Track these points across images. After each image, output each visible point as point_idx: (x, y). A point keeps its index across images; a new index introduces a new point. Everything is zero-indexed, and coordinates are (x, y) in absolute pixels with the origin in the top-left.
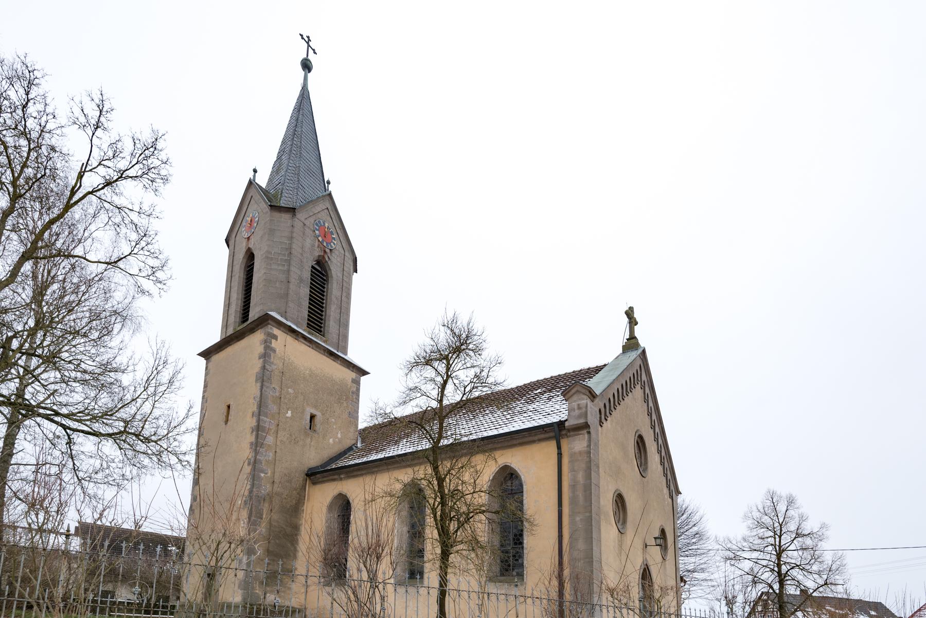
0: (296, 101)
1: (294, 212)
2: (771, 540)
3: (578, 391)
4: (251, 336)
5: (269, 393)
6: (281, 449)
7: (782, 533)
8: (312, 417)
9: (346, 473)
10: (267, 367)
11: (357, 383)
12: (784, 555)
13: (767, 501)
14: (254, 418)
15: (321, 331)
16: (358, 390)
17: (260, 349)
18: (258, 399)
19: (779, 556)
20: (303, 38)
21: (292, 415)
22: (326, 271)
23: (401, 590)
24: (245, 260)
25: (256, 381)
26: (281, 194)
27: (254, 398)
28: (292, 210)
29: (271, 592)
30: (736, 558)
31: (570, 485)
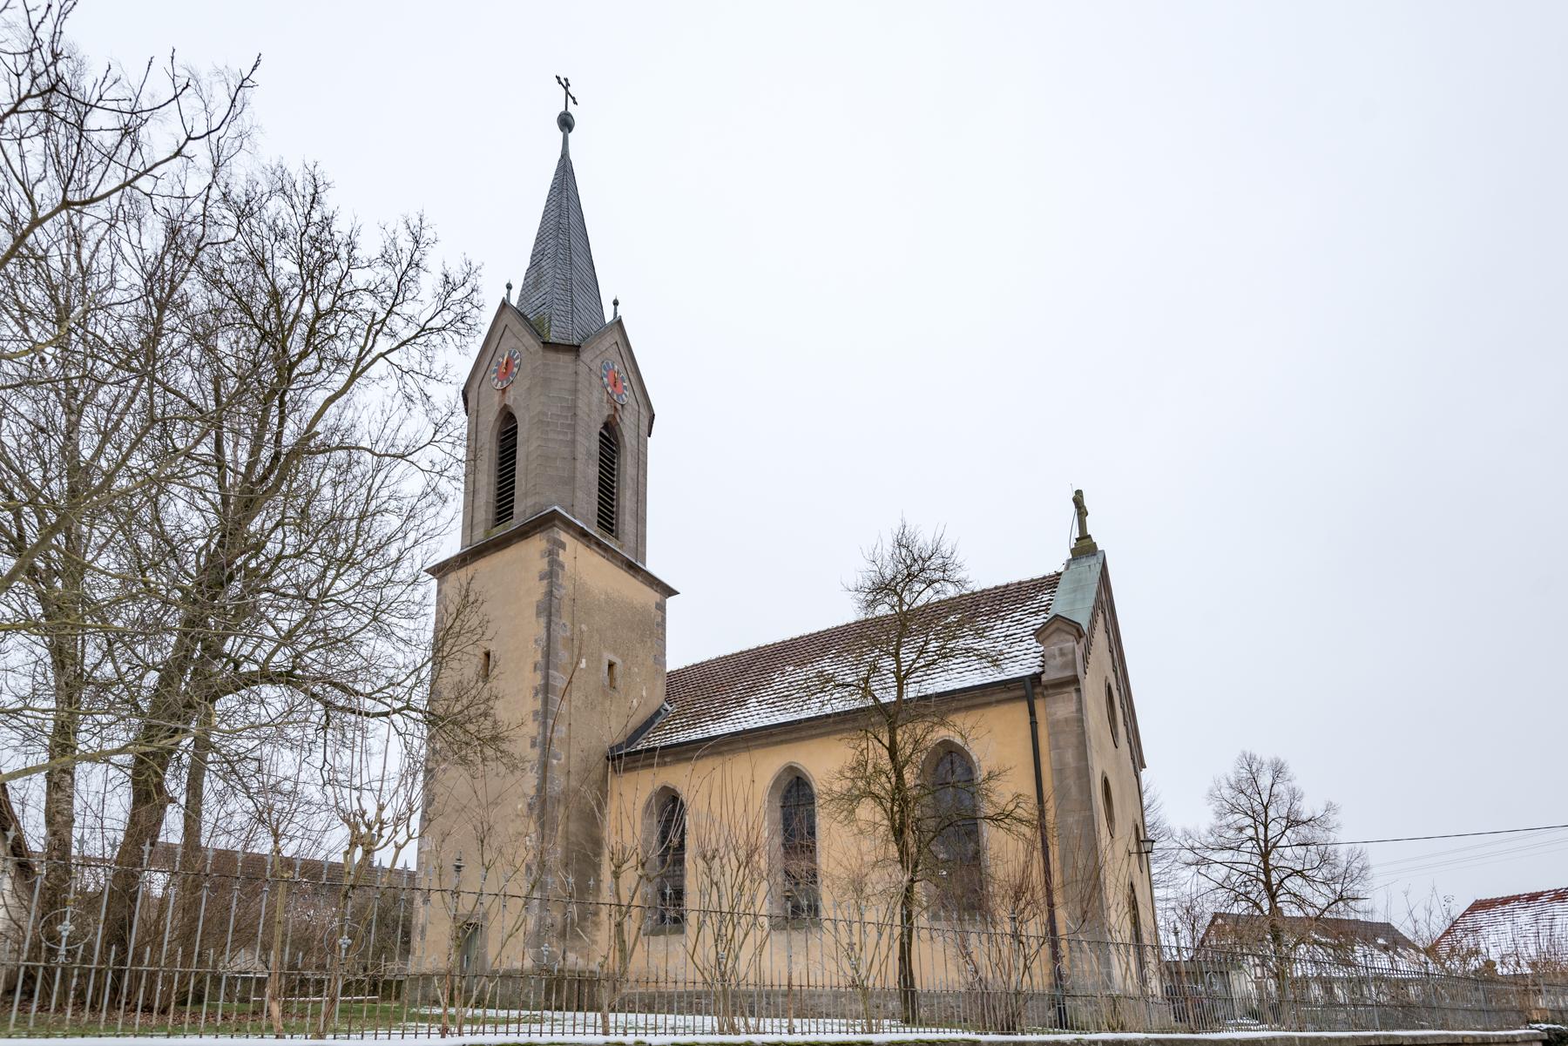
0: (552, 177)
1: (578, 351)
2: (1250, 832)
3: (1058, 629)
4: (523, 543)
5: (560, 634)
6: (575, 720)
7: (1269, 820)
8: (611, 665)
9: (676, 754)
10: (555, 592)
11: (661, 608)
12: (1274, 855)
13: (1242, 771)
14: (538, 672)
15: (612, 531)
16: (664, 619)
17: (543, 565)
18: (543, 643)
19: (1265, 855)
20: (560, 83)
21: (587, 666)
22: (616, 439)
23: (779, 938)
24: (498, 424)
25: (538, 614)
26: (550, 321)
27: (536, 641)
28: (575, 349)
29: (572, 949)
30: (1206, 862)
31: (1052, 770)
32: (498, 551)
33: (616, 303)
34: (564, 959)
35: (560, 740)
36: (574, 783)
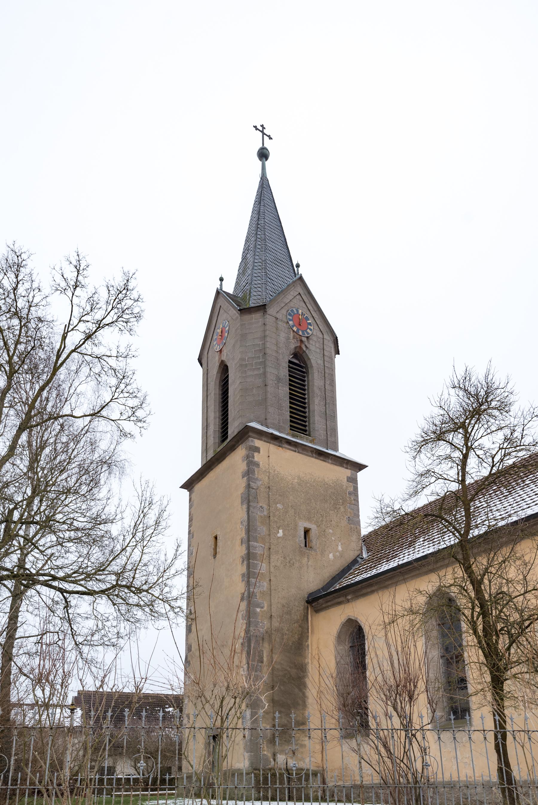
4: (232, 454)
5: (258, 514)
8: (307, 532)
9: (354, 592)
11: (354, 480)
14: (244, 545)
15: (306, 431)
16: (356, 489)
18: (245, 523)
21: (284, 534)
22: (305, 363)
25: (242, 503)
26: (250, 294)
27: (242, 523)
29: (282, 752)
32: (220, 463)
34: (274, 760)
35: (263, 593)
36: (276, 623)
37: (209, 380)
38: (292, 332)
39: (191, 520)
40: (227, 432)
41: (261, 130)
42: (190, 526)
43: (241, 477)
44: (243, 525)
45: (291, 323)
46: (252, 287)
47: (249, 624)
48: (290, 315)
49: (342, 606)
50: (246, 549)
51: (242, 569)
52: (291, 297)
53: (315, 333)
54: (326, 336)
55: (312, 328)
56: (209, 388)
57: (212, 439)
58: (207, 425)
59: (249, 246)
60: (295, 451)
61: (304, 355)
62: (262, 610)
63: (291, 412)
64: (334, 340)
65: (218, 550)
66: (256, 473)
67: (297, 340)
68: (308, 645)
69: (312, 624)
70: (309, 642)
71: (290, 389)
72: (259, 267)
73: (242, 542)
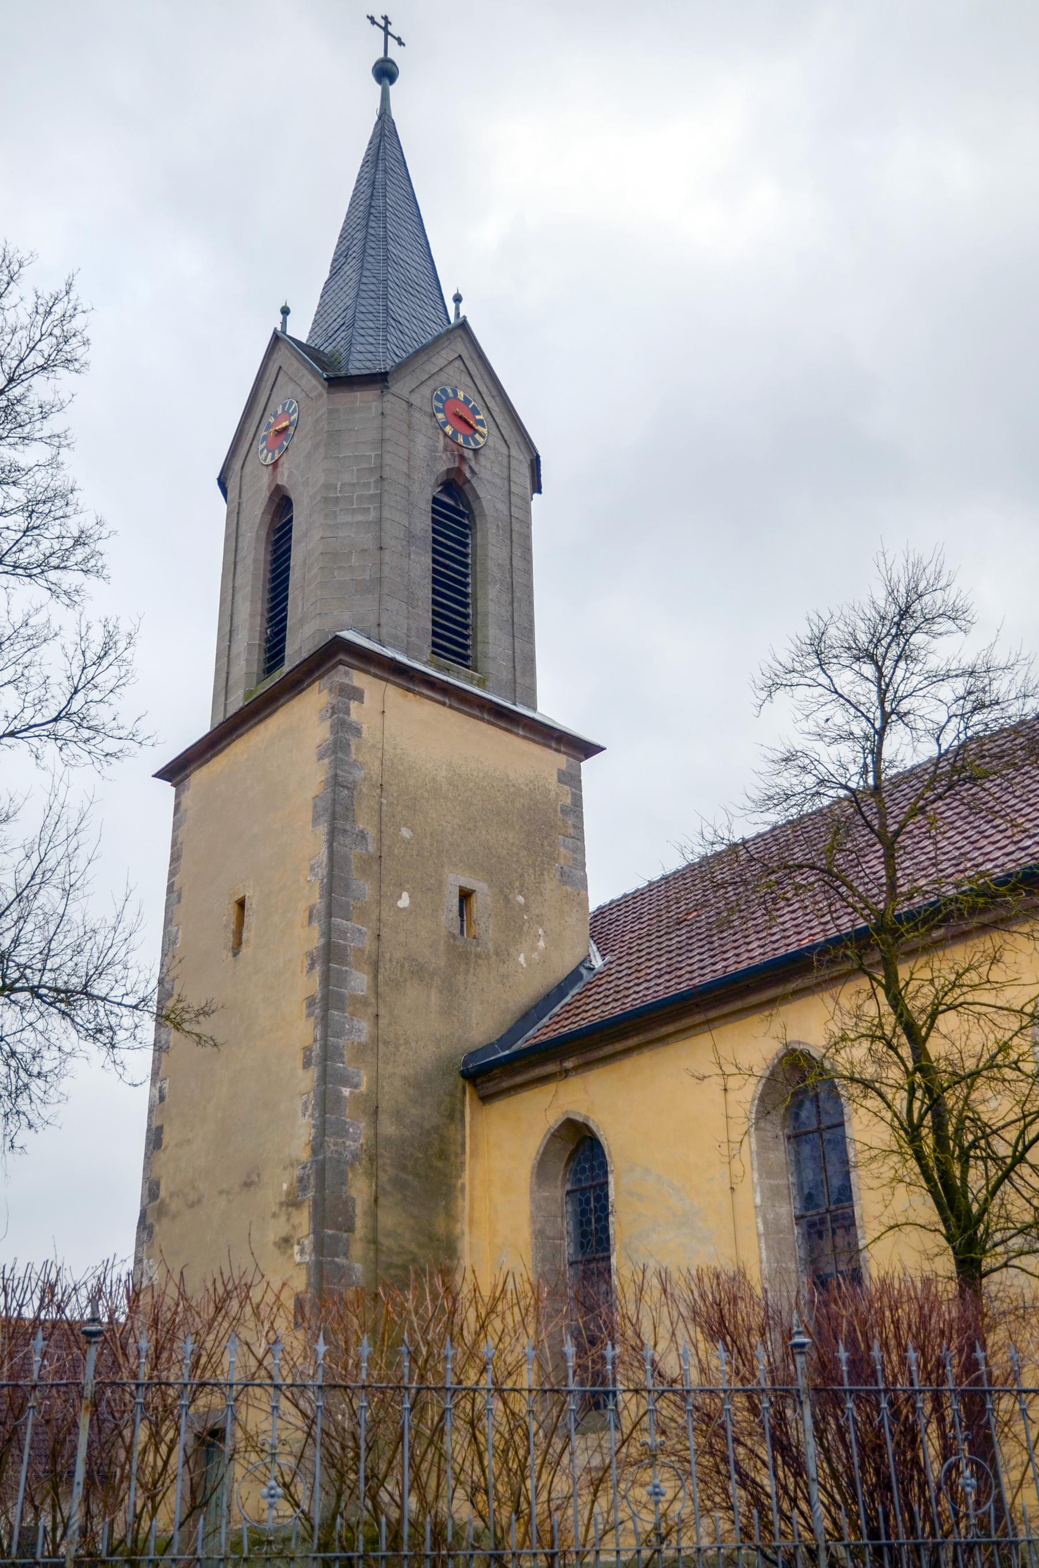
8: (465, 896)
11: (572, 780)
14: (315, 924)
15: (466, 658)
18: (323, 871)
22: (468, 505)
25: (315, 821)
27: (312, 869)
33: (458, 299)
37: (243, 527)
38: (441, 437)
39: (175, 858)
40: (283, 650)
41: (383, 25)
42: (172, 873)
43: (315, 758)
44: (316, 875)
45: (440, 416)
46: (355, 333)
47: (322, 1129)
48: (438, 398)
49: (551, 1087)
50: (322, 935)
51: (311, 984)
52: (442, 362)
53: (490, 443)
54: (514, 452)
55: (485, 431)
56: (240, 545)
57: (243, 663)
58: (231, 631)
59: (348, 248)
60: (444, 704)
61: (466, 487)
62: (357, 1091)
63: (434, 612)
64: (532, 461)
65: (245, 935)
66: (353, 748)
67: (453, 455)
68: (463, 1186)
69: (473, 1134)
70: (466, 1178)
71: (434, 561)
72: (372, 294)
73: (310, 917)
